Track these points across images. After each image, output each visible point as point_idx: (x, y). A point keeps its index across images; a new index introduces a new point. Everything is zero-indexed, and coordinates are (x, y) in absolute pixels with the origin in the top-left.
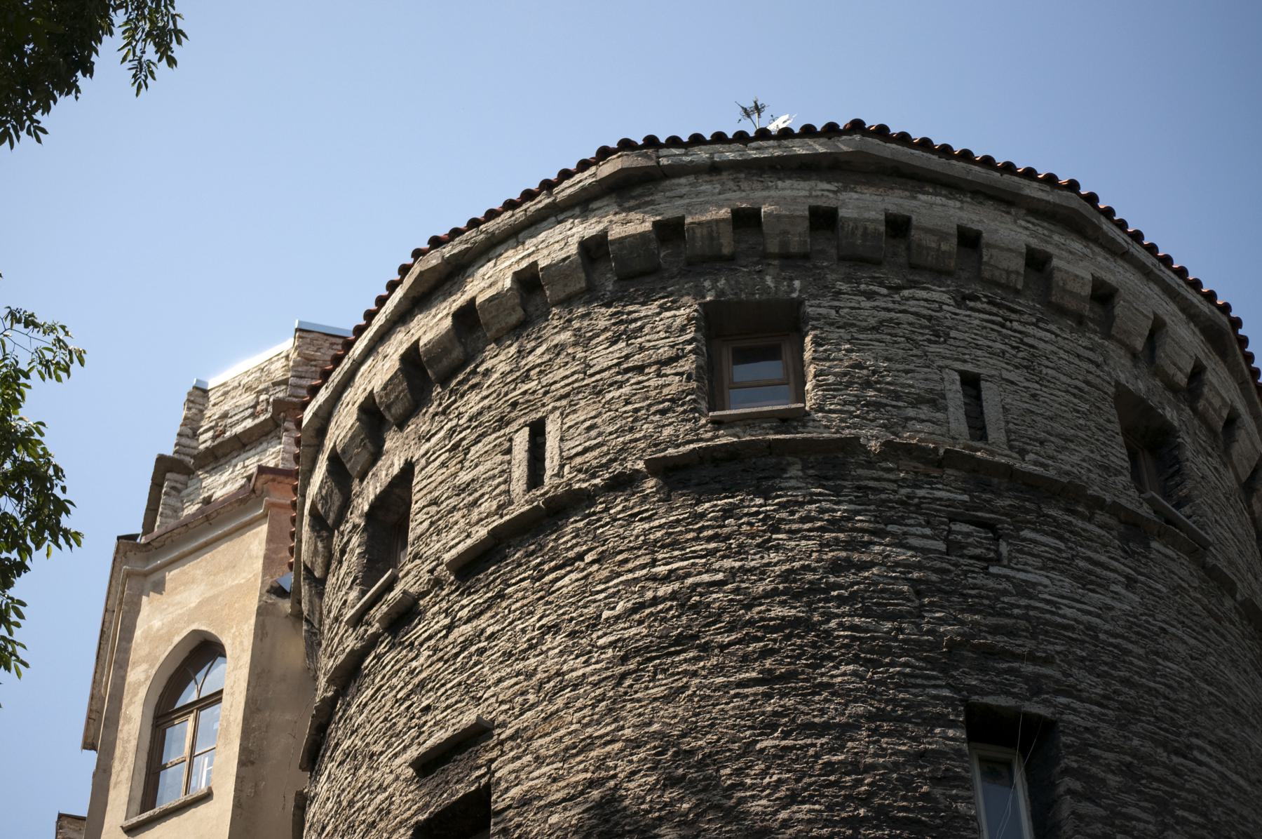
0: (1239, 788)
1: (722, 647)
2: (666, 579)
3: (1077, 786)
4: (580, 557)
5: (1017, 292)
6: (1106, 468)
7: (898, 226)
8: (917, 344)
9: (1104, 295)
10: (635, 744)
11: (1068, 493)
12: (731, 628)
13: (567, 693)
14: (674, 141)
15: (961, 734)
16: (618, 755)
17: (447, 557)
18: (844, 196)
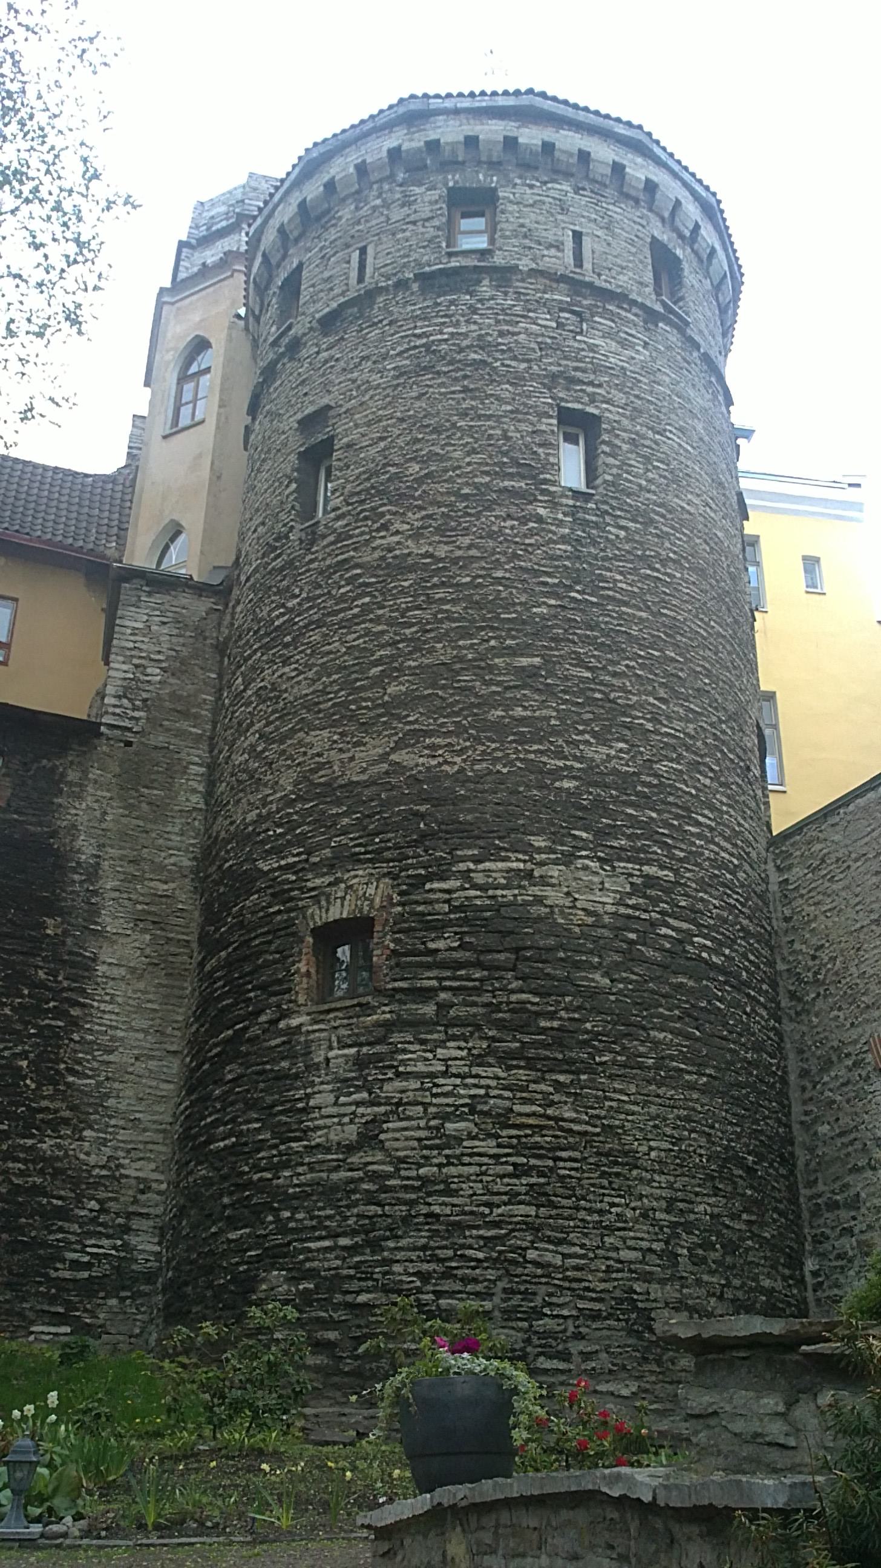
0: (687, 451)
1: (445, 373)
2: (419, 336)
3: (607, 449)
4: (381, 321)
5: (605, 186)
6: (641, 283)
7: (548, 148)
8: (552, 215)
9: (651, 187)
10: (402, 420)
11: (621, 298)
12: (450, 363)
13: (371, 392)
14: (437, 96)
15: (555, 422)
16: (393, 426)
17: (317, 316)
18: (525, 130)
